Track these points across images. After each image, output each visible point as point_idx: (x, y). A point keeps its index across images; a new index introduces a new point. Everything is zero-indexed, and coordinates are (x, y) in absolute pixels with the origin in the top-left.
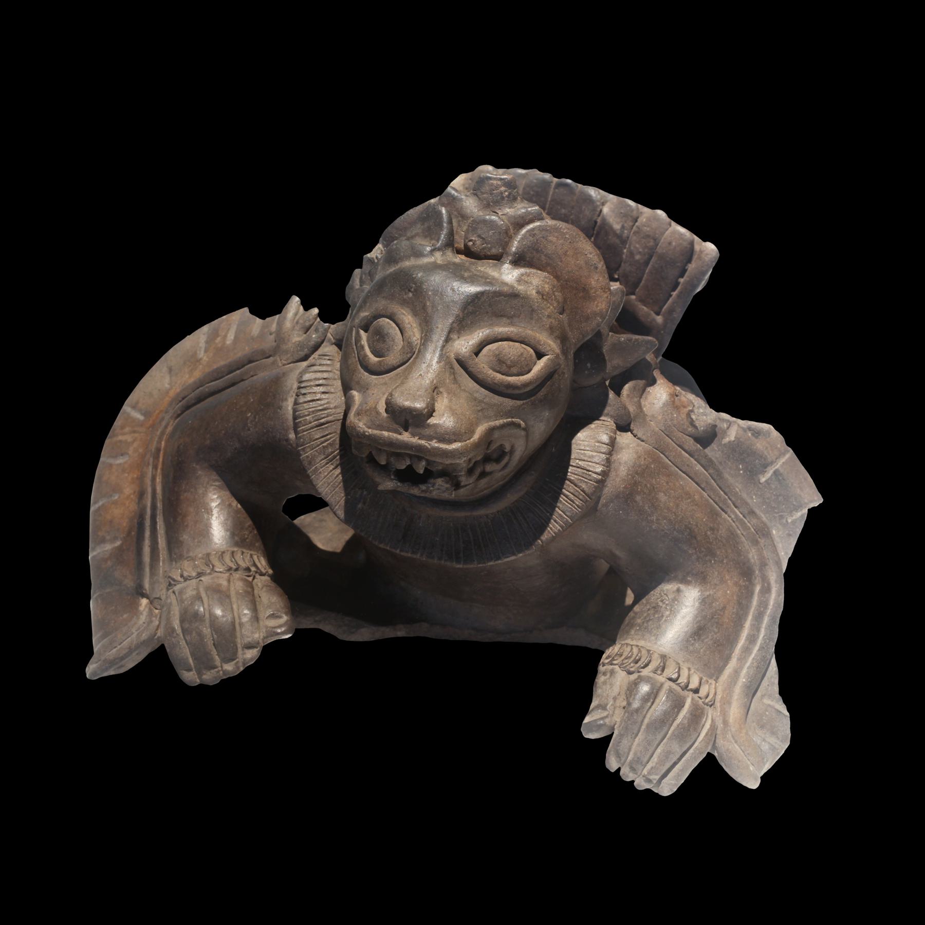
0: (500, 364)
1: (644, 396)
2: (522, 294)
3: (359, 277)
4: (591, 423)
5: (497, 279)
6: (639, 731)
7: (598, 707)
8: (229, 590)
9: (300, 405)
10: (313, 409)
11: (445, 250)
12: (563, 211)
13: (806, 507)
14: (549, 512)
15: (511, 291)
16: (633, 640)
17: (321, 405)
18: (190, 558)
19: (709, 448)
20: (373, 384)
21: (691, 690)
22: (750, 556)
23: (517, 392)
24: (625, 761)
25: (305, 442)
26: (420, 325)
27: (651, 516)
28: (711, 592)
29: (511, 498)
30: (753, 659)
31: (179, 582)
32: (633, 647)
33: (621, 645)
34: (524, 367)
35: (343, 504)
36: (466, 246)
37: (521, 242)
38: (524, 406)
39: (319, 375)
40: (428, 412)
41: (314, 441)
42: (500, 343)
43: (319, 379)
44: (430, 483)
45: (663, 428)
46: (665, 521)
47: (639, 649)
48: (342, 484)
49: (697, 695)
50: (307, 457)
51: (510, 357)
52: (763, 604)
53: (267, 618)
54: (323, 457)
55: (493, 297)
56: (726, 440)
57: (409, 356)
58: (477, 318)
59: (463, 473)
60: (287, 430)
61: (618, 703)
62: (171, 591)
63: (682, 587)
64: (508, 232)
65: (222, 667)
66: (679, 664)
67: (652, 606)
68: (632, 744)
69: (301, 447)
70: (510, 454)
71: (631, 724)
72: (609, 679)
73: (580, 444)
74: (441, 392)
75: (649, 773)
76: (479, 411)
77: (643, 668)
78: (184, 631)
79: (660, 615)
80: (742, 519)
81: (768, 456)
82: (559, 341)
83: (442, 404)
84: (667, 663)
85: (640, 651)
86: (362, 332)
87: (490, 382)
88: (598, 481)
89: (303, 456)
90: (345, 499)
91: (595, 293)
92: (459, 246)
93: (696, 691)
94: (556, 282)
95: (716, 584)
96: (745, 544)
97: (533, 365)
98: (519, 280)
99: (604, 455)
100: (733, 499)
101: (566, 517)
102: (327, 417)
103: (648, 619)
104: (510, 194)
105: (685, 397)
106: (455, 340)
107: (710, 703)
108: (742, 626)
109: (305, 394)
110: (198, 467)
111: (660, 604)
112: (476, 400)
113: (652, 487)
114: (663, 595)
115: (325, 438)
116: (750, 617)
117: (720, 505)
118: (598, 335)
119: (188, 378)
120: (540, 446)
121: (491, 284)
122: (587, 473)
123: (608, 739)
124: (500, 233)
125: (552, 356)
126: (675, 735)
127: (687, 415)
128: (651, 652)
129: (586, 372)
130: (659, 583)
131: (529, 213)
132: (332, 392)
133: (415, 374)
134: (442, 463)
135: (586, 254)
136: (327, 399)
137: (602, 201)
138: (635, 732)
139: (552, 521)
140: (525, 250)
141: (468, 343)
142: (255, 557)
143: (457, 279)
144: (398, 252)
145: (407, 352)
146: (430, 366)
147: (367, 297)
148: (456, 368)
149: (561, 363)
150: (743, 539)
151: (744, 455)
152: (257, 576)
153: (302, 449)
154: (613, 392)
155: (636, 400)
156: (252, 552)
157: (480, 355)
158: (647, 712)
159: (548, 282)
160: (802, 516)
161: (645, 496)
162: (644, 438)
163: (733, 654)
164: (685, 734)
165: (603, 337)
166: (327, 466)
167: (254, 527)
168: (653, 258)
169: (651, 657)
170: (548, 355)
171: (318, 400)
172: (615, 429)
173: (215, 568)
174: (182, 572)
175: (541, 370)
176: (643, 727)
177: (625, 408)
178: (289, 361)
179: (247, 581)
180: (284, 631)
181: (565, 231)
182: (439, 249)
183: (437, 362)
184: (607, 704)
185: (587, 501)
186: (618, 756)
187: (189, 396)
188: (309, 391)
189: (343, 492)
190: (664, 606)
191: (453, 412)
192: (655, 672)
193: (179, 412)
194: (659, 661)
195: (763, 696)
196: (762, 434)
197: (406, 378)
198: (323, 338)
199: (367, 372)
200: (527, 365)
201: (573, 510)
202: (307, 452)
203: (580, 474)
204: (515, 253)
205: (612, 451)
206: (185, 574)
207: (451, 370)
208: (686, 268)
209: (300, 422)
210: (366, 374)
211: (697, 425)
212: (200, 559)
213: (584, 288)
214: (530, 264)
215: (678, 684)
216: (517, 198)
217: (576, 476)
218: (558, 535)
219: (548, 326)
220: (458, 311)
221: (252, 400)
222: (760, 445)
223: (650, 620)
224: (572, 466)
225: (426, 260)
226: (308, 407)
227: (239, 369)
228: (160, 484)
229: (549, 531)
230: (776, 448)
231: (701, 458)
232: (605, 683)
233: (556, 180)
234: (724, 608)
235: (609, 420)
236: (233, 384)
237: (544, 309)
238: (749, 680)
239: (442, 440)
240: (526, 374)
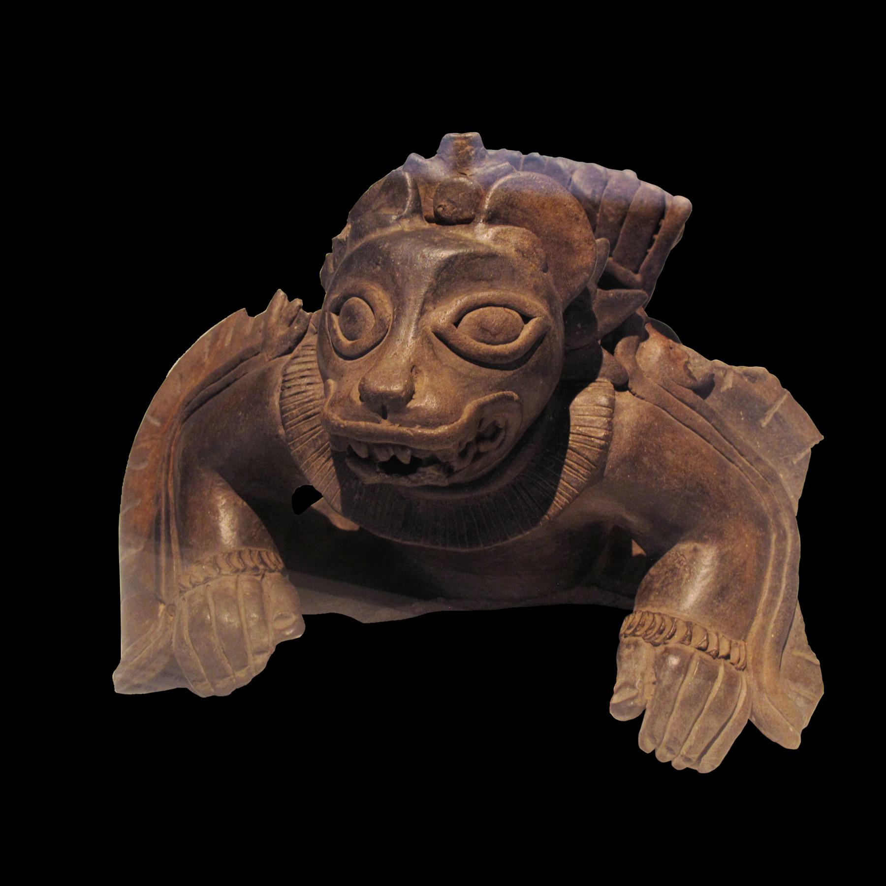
0: (483, 332)
1: (638, 352)
2: (500, 254)
3: (332, 261)
4: (587, 386)
5: (471, 240)
6: (673, 710)
7: (625, 685)
8: (236, 593)
9: (285, 400)
10: (299, 402)
11: (413, 217)
13: (808, 447)
14: (552, 485)
15: (487, 251)
16: (653, 607)
17: (307, 397)
19: (708, 398)
20: (347, 371)
21: (723, 657)
22: (763, 504)
23: (505, 362)
24: (661, 743)
25: (295, 437)
26: (391, 299)
27: (660, 477)
28: (730, 549)
29: (510, 475)
30: (779, 612)
31: (188, 589)
32: (656, 616)
33: (641, 613)
34: (511, 333)
36: (436, 213)
37: (493, 198)
38: (515, 376)
39: (303, 366)
40: (407, 395)
41: (303, 434)
42: (481, 309)
43: (303, 371)
44: (420, 473)
45: (662, 383)
46: (675, 480)
47: (662, 618)
48: (336, 476)
49: (728, 661)
50: (298, 452)
51: (494, 324)
52: (781, 552)
54: (313, 450)
55: (468, 260)
56: (724, 388)
57: (382, 334)
58: (452, 285)
59: (454, 459)
61: (646, 680)
62: (182, 597)
63: (699, 546)
64: (479, 192)
65: (234, 675)
66: (706, 630)
67: (669, 567)
68: (667, 723)
70: (505, 430)
71: (664, 704)
72: (634, 652)
73: (579, 410)
74: (420, 371)
75: (687, 753)
76: (465, 387)
77: (670, 638)
78: (194, 641)
79: (680, 578)
80: (750, 468)
81: (767, 400)
82: (546, 302)
83: (422, 384)
84: (693, 631)
85: (663, 620)
86: (334, 316)
87: (475, 354)
88: (601, 447)
91: (579, 246)
92: (429, 214)
93: (727, 657)
94: (536, 238)
95: (733, 539)
96: (756, 492)
97: (520, 330)
98: (495, 239)
99: (605, 419)
100: (739, 448)
101: (572, 488)
102: (314, 408)
103: (666, 583)
104: (476, 153)
105: (680, 349)
106: (431, 311)
107: (743, 667)
108: (763, 579)
109: (289, 388)
111: (678, 566)
112: (460, 376)
113: (658, 447)
114: (679, 555)
115: (313, 431)
116: (770, 569)
117: (727, 455)
118: (586, 293)
119: (194, 383)
121: (464, 245)
122: (590, 439)
124: (470, 194)
125: (540, 318)
126: (712, 710)
127: (684, 366)
128: (675, 620)
129: (577, 333)
130: (674, 544)
131: (499, 170)
132: (318, 382)
133: (390, 355)
134: (429, 451)
135: (565, 206)
136: (314, 390)
137: (571, 170)
138: (669, 711)
139: (557, 494)
140: (499, 206)
141: (445, 312)
142: (264, 555)
143: (426, 245)
144: (363, 226)
146: (405, 342)
147: (336, 278)
148: (434, 342)
149: (550, 325)
150: (753, 487)
152: (267, 574)
153: (291, 445)
154: (606, 351)
155: (631, 357)
156: (261, 549)
157: (461, 325)
158: (679, 688)
159: (528, 238)
160: (807, 455)
161: (652, 457)
162: (643, 395)
164: (723, 708)
165: (591, 295)
166: (319, 458)
167: (262, 523)
168: (627, 218)
169: (675, 626)
170: (535, 317)
171: (303, 392)
172: (613, 389)
173: (222, 571)
175: (529, 335)
176: (677, 705)
177: (620, 366)
178: (274, 356)
179: (254, 580)
180: (293, 633)
181: (540, 182)
182: (406, 217)
183: (413, 338)
184: (635, 682)
185: (592, 469)
186: (652, 737)
187: (194, 400)
188: (294, 384)
189: (338, 484)
190: (682, 568)
191: (436, 392)
192: (682, 641)
193: (185, 417)
194: (686, 629)
196: (758, 378)
197: (380, 359)
198: (305, 329)
199: (341, 357)
200: (514, 330)
201: (578, 480)
202: (297, 447)
203: (582, 441)
204: (488, 211)
205: (613, 413)
206: (193, 580)
207: (430, 345)
208: (660, 224)
209: (287, 416)
210: (341, 360)
212: (207, 562)
213: (566, 242)
214: (506, 222)
215: (709, 653)
216: (485, 156)
217: (577, 444)
218: (566, 507)
219: (532, 286)
220: (431, 279)
221: (242, 399)
222: (757, 389)
223: (669, 584)
224: (573, 433)
225: (392, 230)
226: (293, 400)
227: (233, 369)
228: (172, 488)
229: (555, 506)
230: (774, 390)
231: (702, 409)
232: (629, 657)
233: (524, 156)
234: (745, 563)
235: (606, 380)
236: (228, 385)
237: (526, 268)
238: (778, 634)
239: (426, 424)
240: (514, 340)
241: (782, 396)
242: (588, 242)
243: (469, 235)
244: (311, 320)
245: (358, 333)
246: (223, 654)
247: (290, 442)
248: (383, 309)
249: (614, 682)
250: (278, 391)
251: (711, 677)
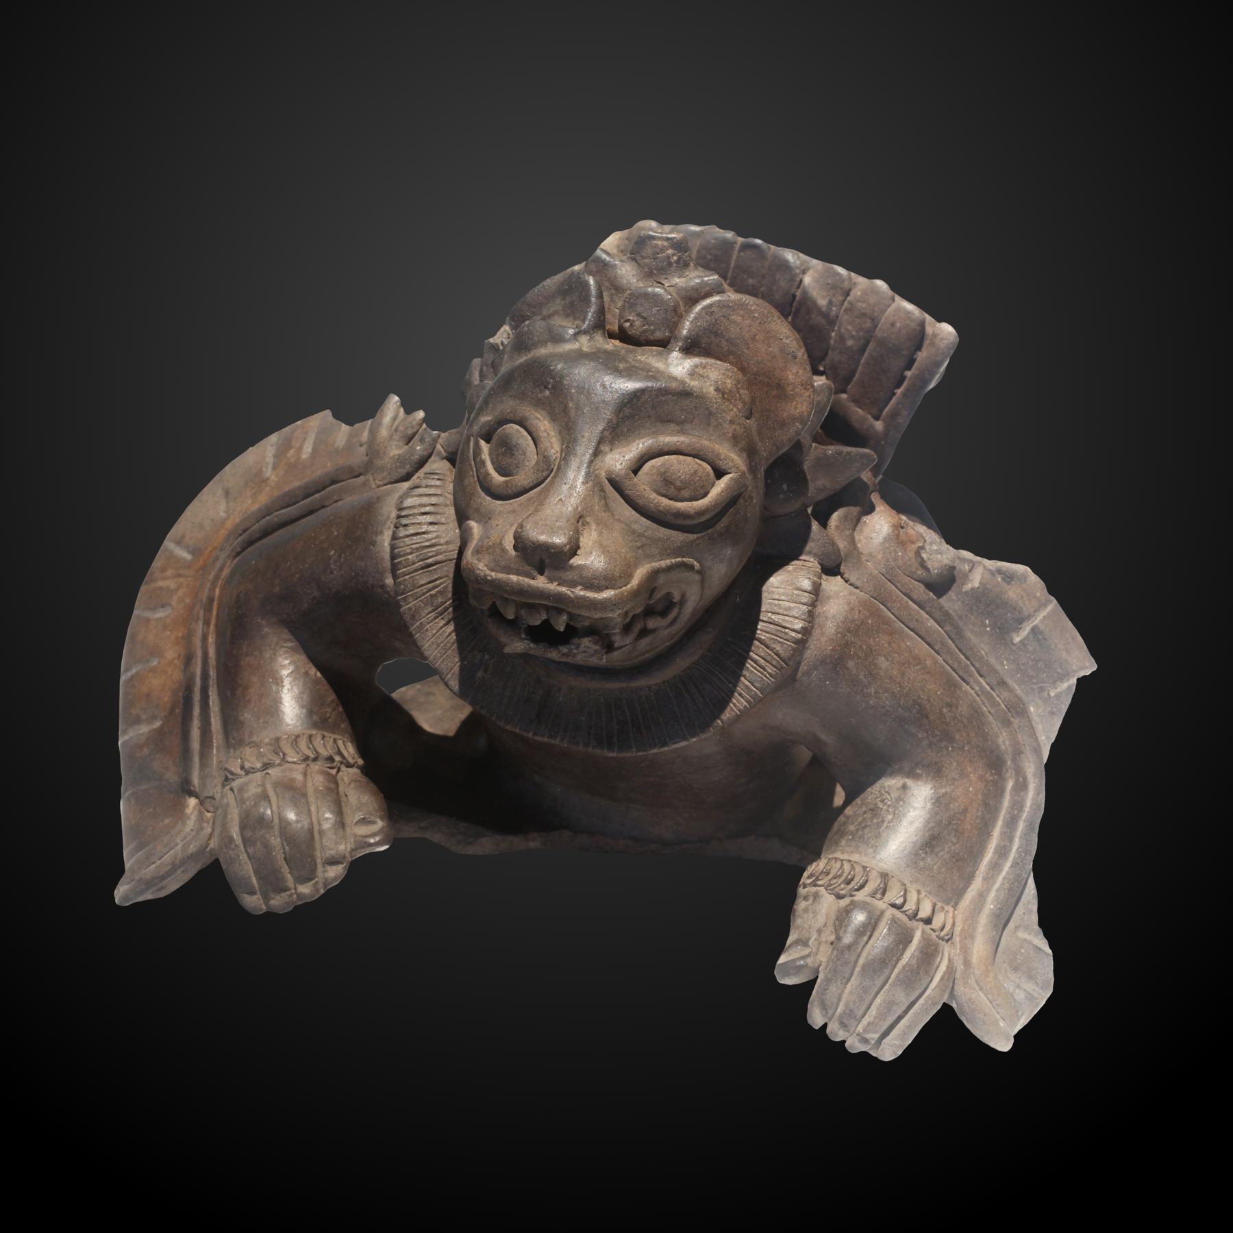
0: (666, 485)
1: (858, 528)
2: (696, 392)
3: (478, 369)
4: (787, 564)
5: (663, 372)
6: (852, 974)
7: (797, 942)
8: (305, 786)
9: (400, 540)
10: (417, 545)
11: (593, 334)
12: (751, 281)
13: (1074, 676)
14: (731, 683)
15: (681, 388)
16: (843, 853)
17: (428, 540)
18: (253, 744)
19: (944, 597)
20: (497, 512)
21: (921, 920)
22: (1000, 741)
23: (689, 522)
24: (833, 1015)
25: (407, 590)
26: (560, 433)
27: (867, 688)
28: (948, 790)
29: (681, 664)
30: (1004, 878)
31: (239, 776)
32: (844, 862)
33: (827, 859)
34: (699, 489)
35: (458, 672)
36: (621, 327)
37: (694, 322)
38: (698, 541)
39: (425, 500)
40: (571, 549)
41: (419, 587)
42: (667, 457)
43: (425, 506)
44: (573, 644)
45: (884, 571)
46: (886, 694)
47: (852, 865)
48: (455, 645)
50: (410, 609)
51: (680, 476)
52: (1018, 806)
53: (355, 824)
54: (430, 609)
55: (657, 396)
56: (968, 587)
57: (545, 474)
58: (636, 424)
59: (617, 631)
60: (382, 574)
61: (824, 938)
62: (228, 787)
63: (909, 782)
64: (677, 309)
65: (296, 889)
66: (905, 885)
68: (843, 992)
70: (680, 605)
71: (842, 966)
72: (812, 905)
73: (773, 592)
74: (588, 523)
75: (865, 1031)
76: (638, 548)
77: (858, 890)
78: (246, 841)
79: (880, 820)
80: (989, 692)
81: (1024, 608)
82: (745, 455)
83: (589, 539)
84: (889, 884)
85: (853, 868)
86: (482, 443)
87: (654, 510)
88: (797, 642)
89: (404, 608)
90: (460, 665)
91: (793, 391)
92: (612, 327)
93: (928, 921)
94: (741, 376)
95: (954, 779)
96: (994, 724)
97: (710, 486)
98: (692, 374)
99: (805, 607)
100: (977, 665)
101: (754, 689)
102: (436, 555)
103: (863, 825)
105: (914, 529)
106: (606, 453)
107: (947, 938)
108: (989, 835)
109: (406, 525)
110: (263, 622)
111: (880, 805)
112: (634, 534)
113: (869, 650)
114: (884, 793)
115: (433, 584)
116: (1000, 823)
117: (960, 673)
118: (798, 446)
119: (251, 504)
120: (720, 595)
121: (654, 378)
122: (783, 630)
123: (810, 985)
124: (666, 310)
125: (736, 475)
126: (899, 980)
127: (915, 553)
128: (868, 870)
129: (782, 496)
130: (878, 777)
131: (705, 284)
132: (443, 522)
133: (553, 499)
134: (589, 618)
135: (781, 339)
136: (436, 532)
137: (803, 268)
138: (847, 975)
139: (736, 694)
140: (700, 333)
141: (624, 457)
142: (340, 743)
143: (609, 372)
144: (530, 336)
145: (542, 469)
146: (573, 487)
147: (489, 396)
148: (607, 491)
149: (748, 484)
150: (991, 718)
151: (992, 606)
152: (343, 768)
153: (402, 599)
154: (816, 523)
155: (847, 533)
157: (640, 473)
158: (862, 949)
159: (731, 377)
160: (1069, 687)
161: (860, 661)
162: (858, 583)
163: (977, 872)
164: (913, 978)
165: (804, 450)
166: (436, 621)
167: (339, 702)
168: (871, 344)
169: (867, 875)
170: (730, 473)
171: (423, 533)
172: (820, 571)
175: (721, 493)
176: (858, 969)
177: (833, 544)
178: (386, 482)
179: (329, 774)
180: (379, 841)
181: (753, 308)
182: (585, 332)
183: (583, 482)
184: (809, 939)
185: (782, 667)
186: (824, 1007)
187: (252, 528)
188: (413, 522)
189: (457, 656)
190: (885, 807)
191: (604, 550)
192: (873, 895)
193: (239, 549)
194: (879, 881)
195: (1017, 928)
196: (1016, 579)
197: (542, 504)
198: (430, 451)
199: (489, 496)
200: (703, 486)
201: (764, 680)
202: (409, 603)
203: (773, 632)
204: (687, 338)
205: (816, 601)
206: (247, 765)
207: (601, 493)
208: (915, 357)
209: (400, 562)
210: (488, 498)
212: (266, 745)
213: (778, 384)
214: (707, 353)
215: (904, 912)
216: (689, 264)
217: (767, 635)
218: (744, 713)
219: (730, 434)
220: (610, 415)
221: (336, 533)
222: (1013, 593)
223: (866, 826)
224: (763, 621)
225: (568, 347)
226: (410, 542)
227: (318, 492)
228: (214, 646)
229: (731, 708)
230: (1035, 597)
231: (934, 610)
232: (806, 910)
233: (740, 240)
234: (965, 810)
235: (812, 560)
236: (311, 512)
237: (725, 412)
238: (998, 906)
239: (589, 586)
240: (701, 499)
241: (1045, 605)
242: (805, 386)
243: (658, 364)
244: (440, 440)
246: (284, 862)
247: (401, 595)
248: (549, 444)
249: (787, 935)
251: (904, 939)
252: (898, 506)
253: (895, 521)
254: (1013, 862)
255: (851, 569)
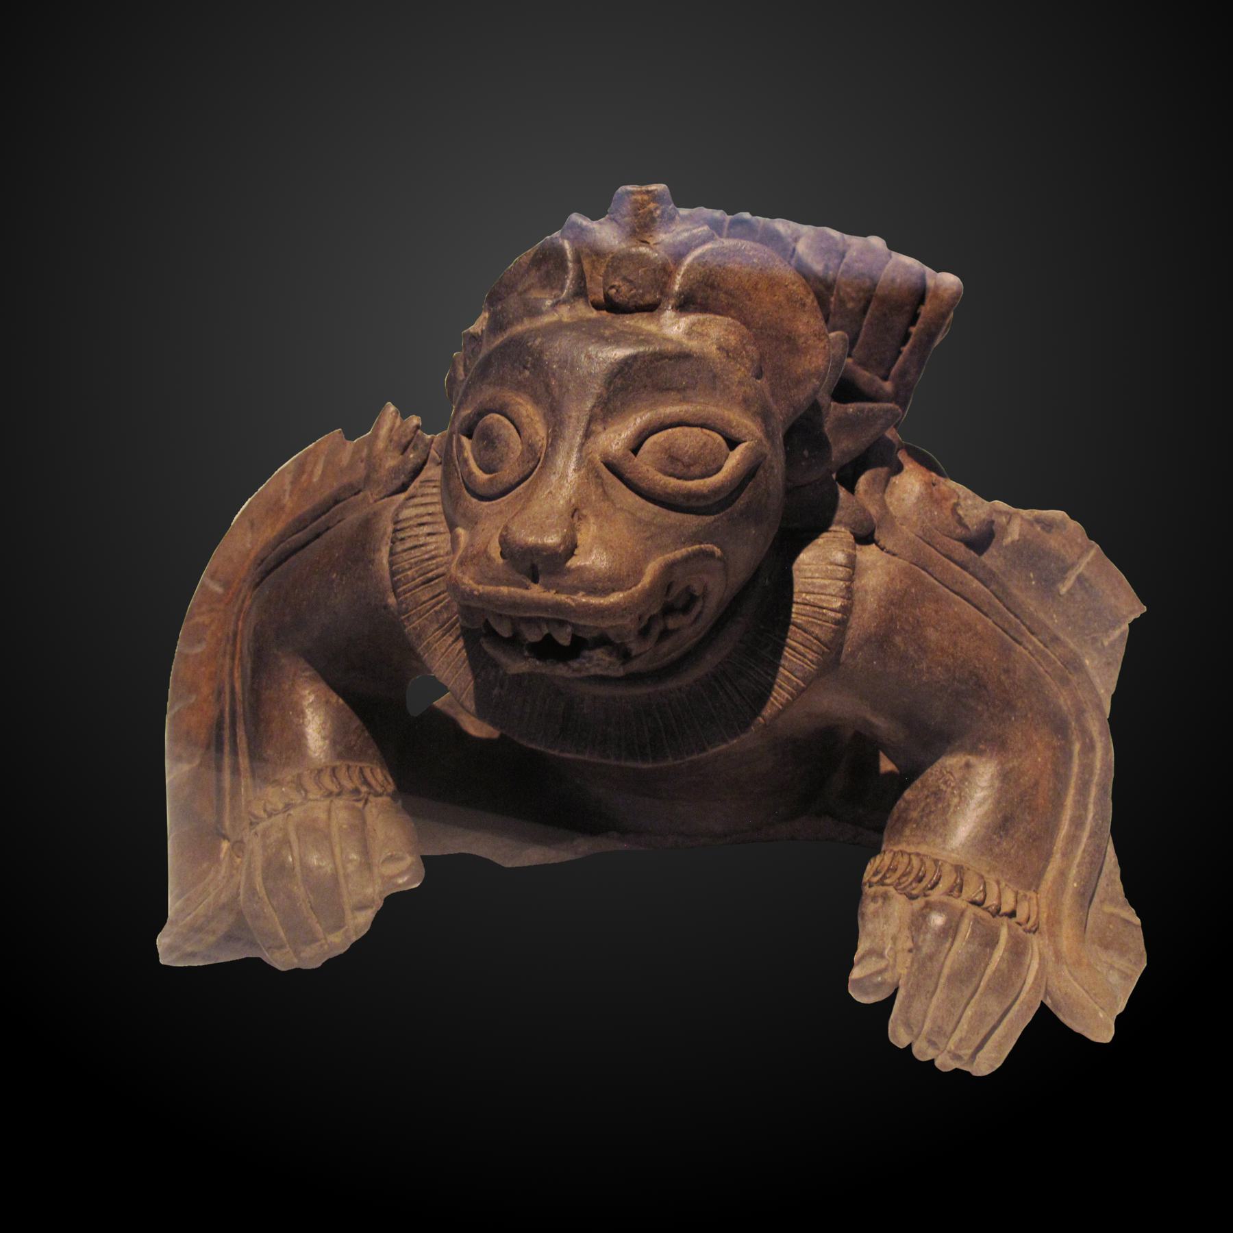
0: (672, 463)
1: (888, 490)
2: (696, 353)
3: (462, 363)
4: (817, 537)
5: (656, 335)
6: (936, 988)
7: (870, 953)
8: (329, 826)
9: (397, 556)
10: (416, 559)
11: (574, 302)
14: (769, 674)
15: (678, 349)
16: (909, 844)
17: (427, 553)
19: (985, 554)
20: (484, 516)
21: (1006, 914)
22: (1061, 701)
23: (702, 503)
24: (919, 1033)
25: (410, 608)
26: (545, 416)
27: (918, 664)
28: (1016, 763)
29: (710, 661)
30: (1084, 851)
31: (262, 819)
32: (913, 857)
33: (892, 853)
34: (711, 463)
36: (606, 296)
37: (686, 276)
38: (716, 524)
39: (422, 510)
40: (566, 549)
41: (422, 604)
42: (670, 430)
43: (422, 516)
44: (584, 658)
45: (921, 533)
46: (939, 668)
47: (922, 860)
48: (467, 662)
49: (1014, 920)
50: (415, 628)
51: (688, 451)
52: (1087, 768)
53: (384, 861)
54: (436, 626)
55: (651, 362)
56: (1008, 540)
57: (531, 465)
58: (630, 396)
59: (632, 639)
61: (899, 946)
62: (253, 831)
63: (972, 759)
64: (666, 268)
65: (325, 939)
66: (982, 877)
67: (931, 790)
68: (928, 1006)
69: (404, 615)
70: (703, 598)
71: (924, 979)
72: (882, 907)
73: (805, 570)
74: (585, 517)
75: (957, 1047)
76: (648, 539)
77: (932, 888)
78: (269, 892)
79: (946, 804)
80: (1044, 651)
81: (1067, 556)
82: (759, 420)
83: (587, 534)
84: (965, 878)
85: (923, 863)
86: (464, 440)
87: (661, 493)
88: (837, 622)
90: (570, 606)
91: (806, 343)
92: (597, 297)
93: (1012, 914)
94: (745, 331)
95: (1021, 751)
96: (1052, 685)
97: (724, 459)
98: (689, 333)
99: (842, 583)
100: (1028, 623)
101: (795, 679)
102: (437, 568)
103: (927, 811)
105: (946, 485)
106: (599, 433)
107: (1034, 929)
108: (1062, 805)
109: (402, 539)
111: (943, 787)
112: (640, 523)
113: (916, 622)
114: (945, 773)
115: (436, 599)
116: (1072, 791)
117: (1012, 634)
118: (815, 407)
119: (269, 533)
120: (860, 905)
121: (646, 341)
122: (821, 611)
124: (655, 270)
125: (752, 442)
126: (990, 988)
127: (952, 509)
128: (940, 863)
129: (803, 464)
130: (938, 757)
131: (694, 237)
132: (442, 531)
133: (543, 494)
134: (597, 628)
135: (786, 286)
136: (437, 542)
137: (794, 236)
138: (931, 989)
139: (776, 687)
140: (694, 287)
141: (620, 435)
142: (368, 773)
143: (593, 341)
144: (505, 314)
146: (564, 476)
147: (468, 387)
148: (605, 476)
149: (766, 452)
150: (1048, 678)
151: (1034, 558)
152: (371, 798)
153: (405, 619)
154: (844, 489)
155: (878, 496)
157: (641, 452)
158: (946, 958)
159: (735, 332)
160: (1123, 633)
161: (907, 635)
162: (895, 550)
163: (1055, 848)
164: (1006, 985)
165: (823, 410)
166: (444, 638)
167: (364, 728)
168: (872, 303)
169: (940, 871)
170: (745, 441)
171: (422, 545)
172: (853, 541)
174: (265, 805)
175: (736, 466)
176: (942, 981)
177: (863, 510)
178: (382, 495)
179: (353, 808)
180: (407, 881)
181: (751, 253)
182: (564, 302)
183: (574, 470)
184: (884, 949)
185: (824, 652)
186: (908, 1025)
187: (270, 557)
188: (409, 534)
189: (470, 674)
190: (949, 790)
191: (606, 545)
192: (949, 892)
193: (258, 580)
194: (955, 876)
195: (1102, 902)
196: (1055, 526)
197: (529, 500)
198: (425, 457)
199: (474, 497)
200: (715, 459)
201: (805, 668)
202: (414, 623)
203: (810, 614)
204: (680, 294)
205: (853, 574)
206: (269, 808)
207: (598, 480)
208: (918, 311)
209: (400, 579)
210: (474, 500)
211: (968, 523)
212: (288, 783)
214: (704, 308)
215: (986, 909)
216: (674, 217)
217: (804, 618)
218: (787, 705)
219: (741, 398)
220: (599, 389)
221: (337, 555)
222: (1053, 542)
223: (931, 812)
224: (797, 603)
225: (546, 319)
226: (408, 557)
227: (324, 513)
228: (240, 680)
229: (773, 704)
230: (1077, 543)
231: (977, 570)
232: (876, 914)
233: (729, 218)
234: (1036, 784)
235: (843, 529)
236: (318, 536)
237: (732, 373)
238: (1082, 883)
239: (592, 591)
240: (715, 474)
243: (652, 328)
244: (433, 445)
245: (498, 464)
249: (856, 949)
250: (387, 544)
252: (926, 463)
253: (926, 478)
254: (1091, 833)
255: (886, 536)
